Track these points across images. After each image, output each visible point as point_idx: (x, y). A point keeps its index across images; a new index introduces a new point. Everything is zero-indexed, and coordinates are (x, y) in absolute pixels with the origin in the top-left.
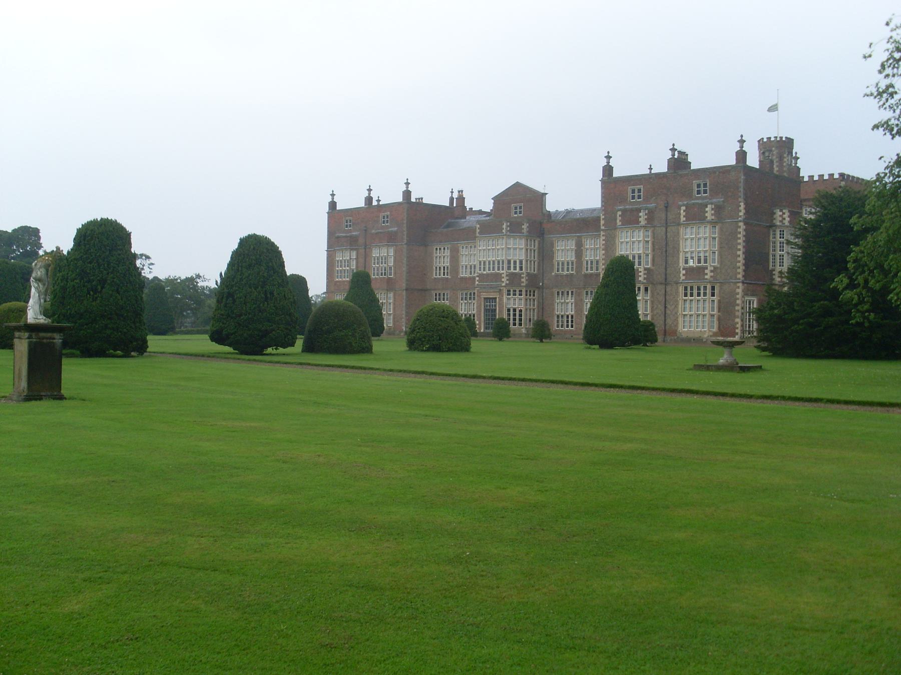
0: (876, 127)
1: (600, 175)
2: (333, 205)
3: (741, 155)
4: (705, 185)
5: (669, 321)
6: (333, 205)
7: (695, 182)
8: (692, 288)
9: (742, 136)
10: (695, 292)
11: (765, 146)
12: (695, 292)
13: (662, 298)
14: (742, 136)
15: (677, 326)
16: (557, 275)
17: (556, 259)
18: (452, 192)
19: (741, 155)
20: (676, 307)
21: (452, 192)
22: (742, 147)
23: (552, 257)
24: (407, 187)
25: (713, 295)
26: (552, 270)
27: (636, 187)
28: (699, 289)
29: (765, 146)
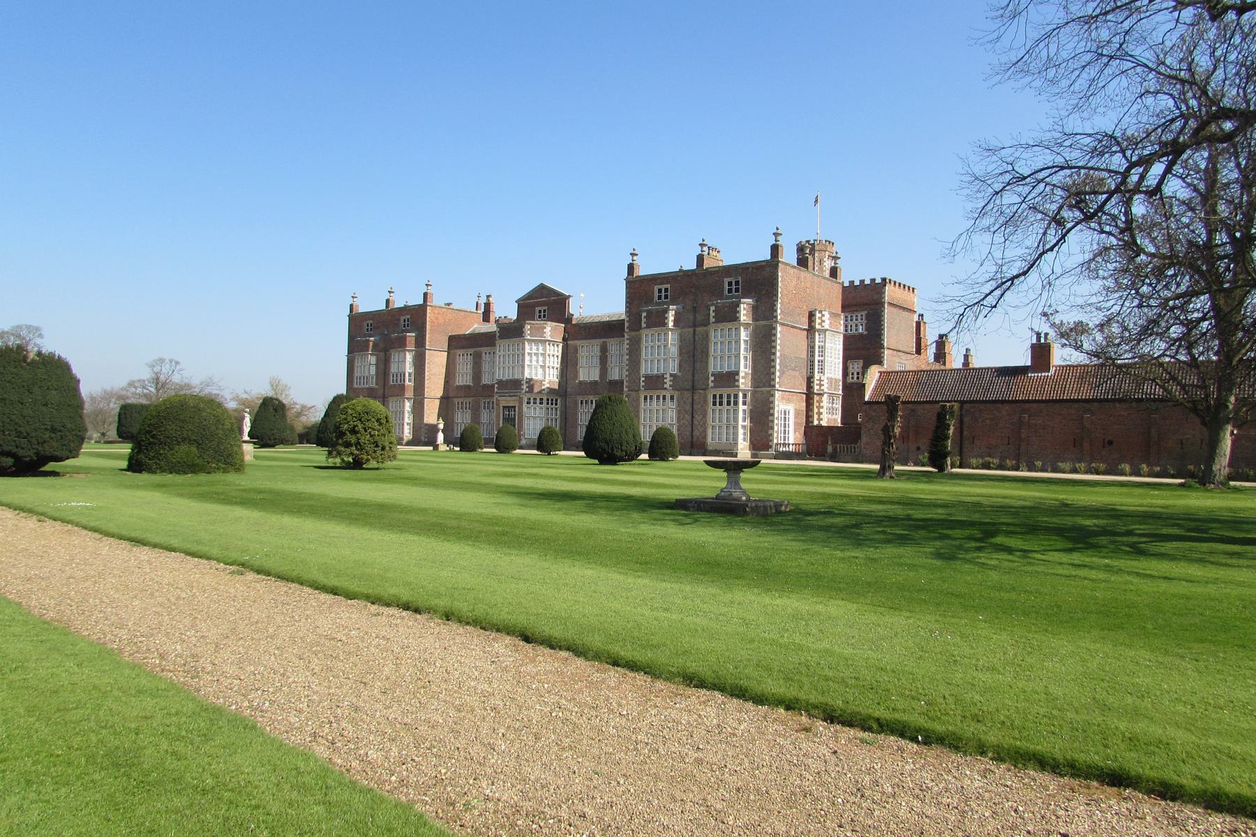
4: (737, 283)
5: (696, 433)
6: (631, 268)
8: (721, 396)
10: (725, 400)
12: (725, 400)
13: (688, 408)
15: (705, 437)
20: (705, 415)
25: (744, 403)
28: (729, 396)
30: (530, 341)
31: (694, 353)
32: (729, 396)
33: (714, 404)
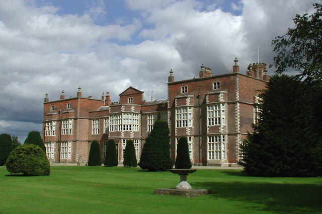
25: (224, 140)
30: (125, 114)
31: (201, 118)
33: (210, 141)
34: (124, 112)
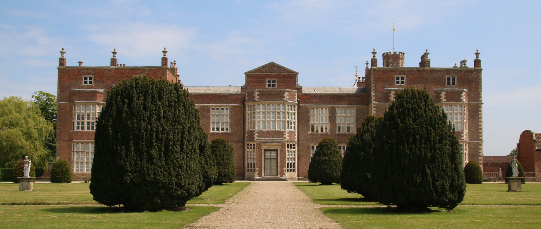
0: (114, 53)
1: (57, 65)
2: (62, 61)
3: (374, 62)
6: (62, 61)
7: (447, 77)
9: (477, 51)
11: (386, 57)
14: (477, 51)
16: (312, 134)
17: (311, 121)
18: (367, 64)
19: (374, 62)
21: (367, 64)
22: (374, 56)
23: (309, 121)
24: (477, 57)
26: (309, 130)
27: (400, 76)
29: (386, 57)
32: (251, 145)
33: (248, 148)
34: (288, 101)
